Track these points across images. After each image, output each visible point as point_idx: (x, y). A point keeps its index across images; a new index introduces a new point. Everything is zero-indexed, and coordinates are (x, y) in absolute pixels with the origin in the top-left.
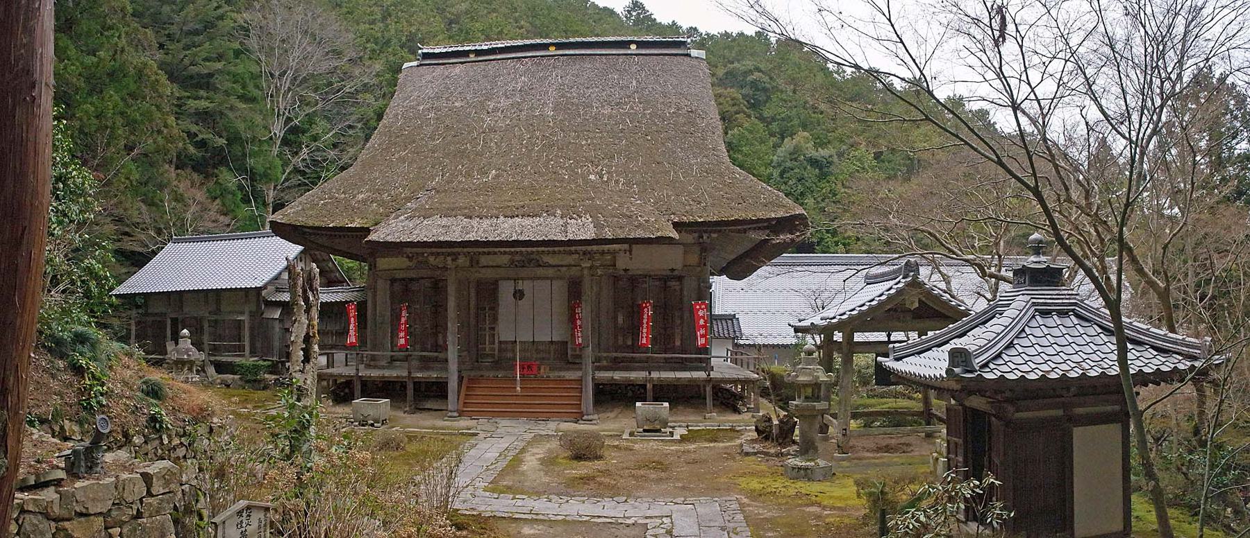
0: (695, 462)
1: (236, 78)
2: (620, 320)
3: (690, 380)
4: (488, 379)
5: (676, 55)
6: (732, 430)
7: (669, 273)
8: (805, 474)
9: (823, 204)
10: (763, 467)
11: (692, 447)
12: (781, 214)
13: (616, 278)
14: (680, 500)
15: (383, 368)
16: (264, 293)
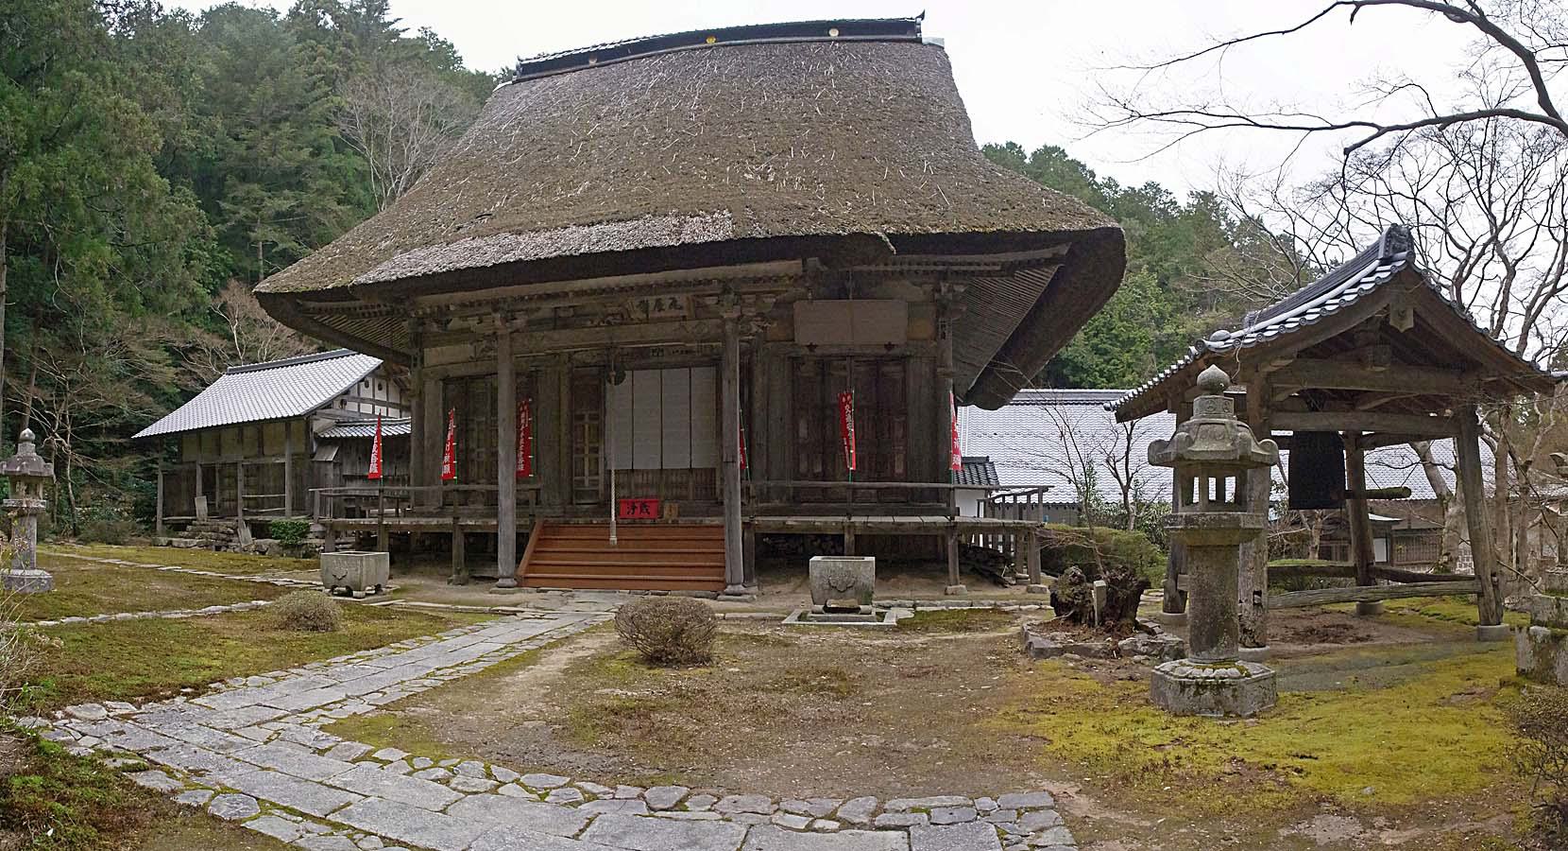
0: (923, 673)
1: (335, 174)
2: (803, 431)
3: (920, 526)
4: (577, 526)
5: (899, 41)
6: (996, 610)
7: (884, 351)
8: (1216, 699)
9: (1095, 341)
10: (1088, 683)
11: (919, 640)
12: (1079, 225)
13: (796, 362)
14: (858, 808)
15: (430, 515)
16: (316, 426)
